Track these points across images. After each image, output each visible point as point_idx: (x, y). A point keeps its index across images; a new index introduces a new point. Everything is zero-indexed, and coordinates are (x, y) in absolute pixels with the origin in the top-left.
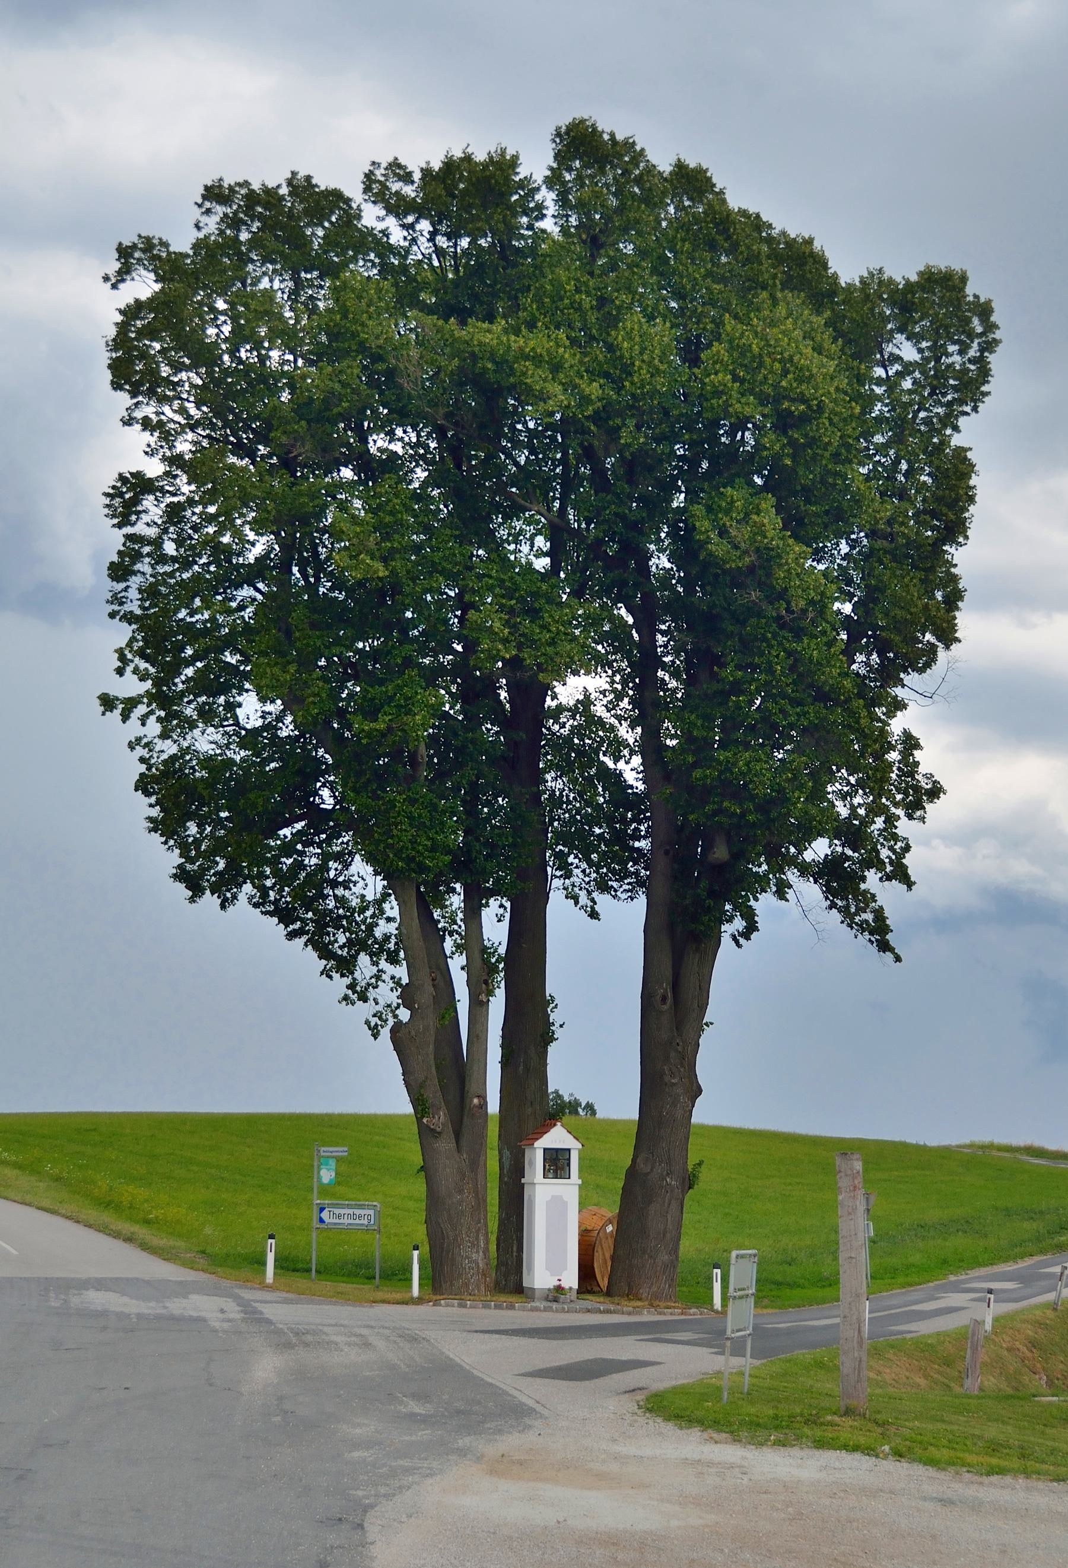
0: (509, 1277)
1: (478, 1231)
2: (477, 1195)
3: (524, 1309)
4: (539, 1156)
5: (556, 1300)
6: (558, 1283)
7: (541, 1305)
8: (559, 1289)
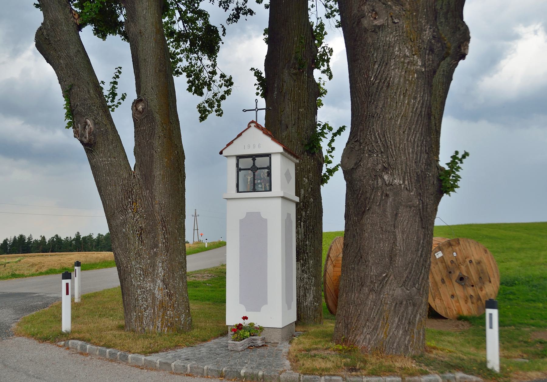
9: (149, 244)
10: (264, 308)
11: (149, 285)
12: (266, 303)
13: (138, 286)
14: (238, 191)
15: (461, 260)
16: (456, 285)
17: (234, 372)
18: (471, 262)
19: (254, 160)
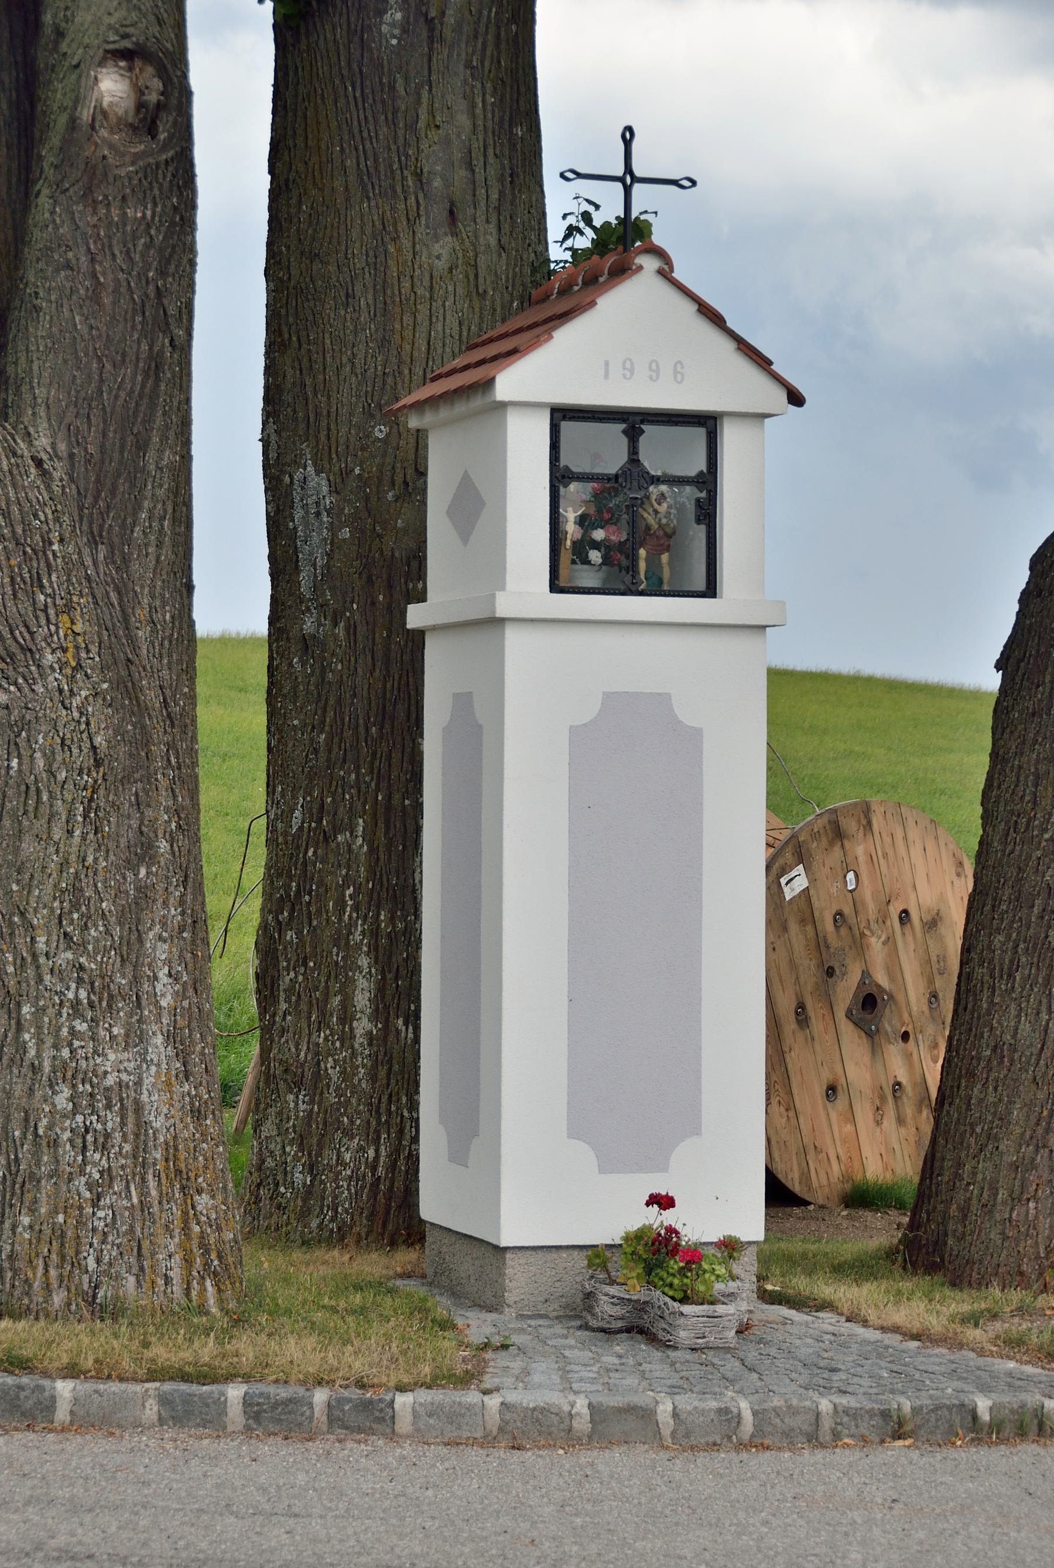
0: (339, 1143)
1: (135, 909)
2: (127, 689)
3: (454, 1434)
4: (526, 451)
5: (641, 1328)
6: (655, 1218)
7: (558, 1377)
8: (659, 1253)
9: (123, 842)
10: (583, 1154)
11: (113, 1064)
12: (697, 1131)
13: (61, 1068)
14: (555, 587)
15: (872, 907)
16: (847, 1028)
17: (950, 1408)
18: (905, 916)
19: (633, 435)
